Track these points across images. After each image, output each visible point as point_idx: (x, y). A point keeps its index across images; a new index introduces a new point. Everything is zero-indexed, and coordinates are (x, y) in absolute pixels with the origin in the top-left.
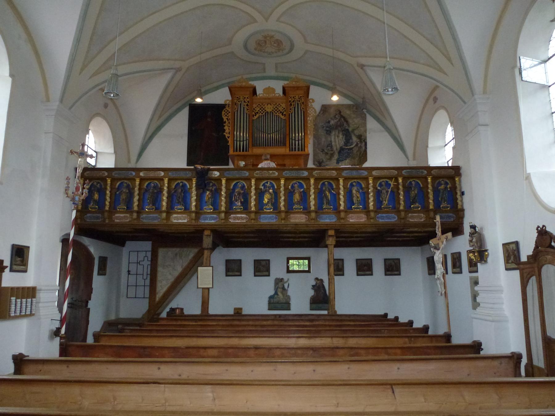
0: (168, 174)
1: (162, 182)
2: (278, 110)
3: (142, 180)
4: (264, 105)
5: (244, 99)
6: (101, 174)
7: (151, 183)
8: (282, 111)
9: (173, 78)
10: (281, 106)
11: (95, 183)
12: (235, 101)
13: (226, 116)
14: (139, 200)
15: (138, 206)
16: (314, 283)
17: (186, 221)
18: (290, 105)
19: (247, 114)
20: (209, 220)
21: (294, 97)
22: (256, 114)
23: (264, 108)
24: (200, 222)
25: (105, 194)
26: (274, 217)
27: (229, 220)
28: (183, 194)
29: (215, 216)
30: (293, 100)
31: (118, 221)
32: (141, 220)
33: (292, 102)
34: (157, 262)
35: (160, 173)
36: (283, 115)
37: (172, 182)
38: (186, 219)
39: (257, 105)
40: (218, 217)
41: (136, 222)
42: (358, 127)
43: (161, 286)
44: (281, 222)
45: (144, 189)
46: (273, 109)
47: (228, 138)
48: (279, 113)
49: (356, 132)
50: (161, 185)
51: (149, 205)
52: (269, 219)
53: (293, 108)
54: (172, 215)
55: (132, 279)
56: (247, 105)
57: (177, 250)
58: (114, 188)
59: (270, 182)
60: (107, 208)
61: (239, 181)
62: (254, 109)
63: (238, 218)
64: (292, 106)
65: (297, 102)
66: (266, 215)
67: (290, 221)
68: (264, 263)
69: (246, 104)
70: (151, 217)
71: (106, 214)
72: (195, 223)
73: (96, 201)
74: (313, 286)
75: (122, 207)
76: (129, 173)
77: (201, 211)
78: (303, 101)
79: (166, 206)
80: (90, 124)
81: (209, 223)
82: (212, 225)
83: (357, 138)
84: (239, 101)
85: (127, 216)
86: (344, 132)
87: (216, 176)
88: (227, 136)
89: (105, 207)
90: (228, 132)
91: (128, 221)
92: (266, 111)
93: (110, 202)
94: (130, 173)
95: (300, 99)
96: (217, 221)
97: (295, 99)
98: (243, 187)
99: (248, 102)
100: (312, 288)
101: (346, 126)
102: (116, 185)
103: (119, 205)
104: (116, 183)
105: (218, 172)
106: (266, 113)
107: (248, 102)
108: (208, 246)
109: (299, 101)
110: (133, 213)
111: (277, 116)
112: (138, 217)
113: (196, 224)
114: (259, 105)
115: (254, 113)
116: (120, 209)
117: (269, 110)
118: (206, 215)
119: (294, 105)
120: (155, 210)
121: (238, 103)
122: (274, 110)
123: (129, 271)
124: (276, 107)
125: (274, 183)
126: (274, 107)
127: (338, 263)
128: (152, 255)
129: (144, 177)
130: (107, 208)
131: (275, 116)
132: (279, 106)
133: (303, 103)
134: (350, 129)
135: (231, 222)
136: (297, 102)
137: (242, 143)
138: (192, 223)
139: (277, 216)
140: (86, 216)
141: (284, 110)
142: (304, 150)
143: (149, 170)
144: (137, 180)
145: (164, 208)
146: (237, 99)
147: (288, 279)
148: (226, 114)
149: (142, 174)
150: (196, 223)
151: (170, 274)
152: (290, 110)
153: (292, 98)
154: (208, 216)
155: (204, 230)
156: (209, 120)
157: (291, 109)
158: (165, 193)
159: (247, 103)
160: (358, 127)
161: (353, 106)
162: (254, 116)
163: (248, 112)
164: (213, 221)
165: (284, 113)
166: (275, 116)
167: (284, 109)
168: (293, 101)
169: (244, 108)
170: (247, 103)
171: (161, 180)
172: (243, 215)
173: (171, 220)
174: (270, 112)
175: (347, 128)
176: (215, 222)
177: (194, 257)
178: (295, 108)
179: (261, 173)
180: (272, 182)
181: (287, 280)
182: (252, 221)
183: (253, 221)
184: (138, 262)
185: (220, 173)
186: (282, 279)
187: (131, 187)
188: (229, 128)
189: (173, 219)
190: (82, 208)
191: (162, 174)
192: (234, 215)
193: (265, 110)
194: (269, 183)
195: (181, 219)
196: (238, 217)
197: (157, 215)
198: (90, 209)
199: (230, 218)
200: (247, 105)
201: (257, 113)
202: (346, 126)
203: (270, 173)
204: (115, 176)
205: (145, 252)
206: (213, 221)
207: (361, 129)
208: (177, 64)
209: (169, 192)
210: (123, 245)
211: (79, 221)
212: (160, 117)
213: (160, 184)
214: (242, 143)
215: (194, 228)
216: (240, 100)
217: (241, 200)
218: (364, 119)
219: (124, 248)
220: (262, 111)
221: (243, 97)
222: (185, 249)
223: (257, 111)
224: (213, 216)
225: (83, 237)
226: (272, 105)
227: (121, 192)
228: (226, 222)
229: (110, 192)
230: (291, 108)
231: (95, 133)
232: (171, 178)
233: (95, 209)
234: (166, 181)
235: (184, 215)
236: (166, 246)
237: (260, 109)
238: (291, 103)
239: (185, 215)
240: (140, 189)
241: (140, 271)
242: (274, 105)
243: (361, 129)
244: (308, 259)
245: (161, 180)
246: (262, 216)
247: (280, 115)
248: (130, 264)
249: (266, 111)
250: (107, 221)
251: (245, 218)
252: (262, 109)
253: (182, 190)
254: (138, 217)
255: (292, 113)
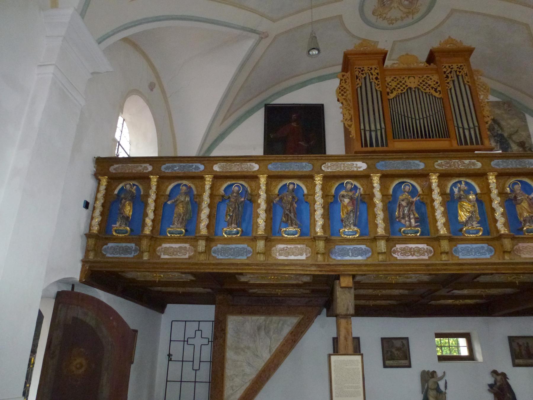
0: (267, 167)
1: (253, 184)
2: (427, 85)
3: (218, 178)
4: (404, 78)
5: (370, 71)
6: (140, 168)
7: (232, 185)
8: (434, 86)
9: (252, 50)
10: (431, 79)
11: (128, 186)
12: (357, 73)
13: (343, 95)
14: (209, 217)
15: (208, 227)
16: (491, 380)
17: (304, 257)
18: (445, 78)
19: (376, 91)
20: (350, 254)
21: (449, 67)
22: (392, 90)
23: (403, 82)
24: (334, 259)
25: (146, 204)
26: (486, 248)
27: (392, 256)
28: (296, 205)
29: (363, 247)
30: (450, 70)
31: (166, 257)
32: (213, 255)
33: (448, 73)
34: (224, 341)
35: (250, 164)
36: (436, 90)
37: (274, 184)
38: (304, 254)
39: (392, 78)
40: (369, 249)
41: (202, 258)
42: (517, 131)
43: (232, 387)
44: (504, 259)
45: (218, 195)
46: (419, 83)
47: (349, 128)
48: (429, 90)
49: (514, 137)
50: (251, 190)
51: (229, 224)
52: (475, 253)
53: (451, 82)
54: (274, 246)
55: (175, 367)
56: (377, 78)
57: (261, 319)
58: (163, 195)
59: (465, 182)
60: (147, 231)
61: (405, 180)
62: (388, 84)
63: (412, 252)
64: (450, 79)
65: (456, 73)
66: (469, 245)
67: (520, 256)
68: (398, 344)
69: (374, 77)
70: (231, 249)
71: (145, 243)
72: (324, 261)
73: (128, 217)
74: (491, 386)
75: (177, 228)
76: (193, 166)
77: (216, 237)
78: (465, 72)
79: (264, 228)
80: (124, 108)
81: (353, 260)
82: (360, 265)
83: (518, 145)
84: (363, 74)
85: (185, 247)
86: (496, 138)
87: (361, 169)
88: (347, 124)
89: (143, 230)
90: (349, 119)
91: (187, 256)
92: (408, 87)
93: (153, 221)
94: (194, 167)
95: (460, 69)
96: (367, 258)
97: (453, 70)
98: (413, 192)
99: (378, 74)
100: (489, 390)
101: (499, 130)
102: (166, 190)
103: (171, 226)
104: (167, 187)
105: (363, 162)
106: (407, 90)
107: (378, 74)
108: (348, 309)
109: (460, 72)
110: (197, 241)
111: (426, 93)
112: (208, 248)
113: (326, 263)
114: (395, 78)
115: (388, 90)
116: (173, 234)
117: (413, 86)
118: (344, 246)
119: (452, 78)
120: (241, 236)
121: (361, 75)
122: (422, 85)
123: (169, 355)
124: (423, 81)
125: (473, 183)
126: (421, 81)
127: (527, 343)
128: (443, 337)
129: (220, 172)
130: (147, 231)
131: (424, 95)
132: (428, 79)
133: (466, 73)
134: (506, 135)
135: (398, 258)
136: (456, 73)
137: (373, 134)
138: (316, 261)
139: (491, 246)
140: (105, 247)
141: (438, 84)
142: (387, 146)
143: (230, 161)
144: (207, 179)
145: (261, 231)
146: (359, 71)
147: (444, 373)
148: (342, 92)
149: (216, 168)
150: (326, 261)
151: (249, 364)
152: (448, 85)
153: (447, 67)
154: (348, 247)
155: (338, 277)
156: (294, 124)
157: (448, 83)
158: (262, 201)
159: (375, 75)
160: (517, 131)
161: (504, 103)
162: (390, 94)
163: (380, 87)
164: (360, 258)
165: (439, 89)
166: (424, 95)
167: (437, 83)
168: (451, 72)
169: (371, 83)
170: (375, 75)
171: (253, 177)
172: (420, 246)
173: (273, 255)
174: (415, 88)
175: (500, 132)
176: (365, 260)
177: (291, 333)
178: (453, 81)
179: (448, 163)
180: (469, 181)
181: (443, 374)
182: (443, 256)
183: (444, 257)
184: (186, 340)
185: (367, 163)
186: (434, 372)
187: (195, 193)
188: (350, 112)
189: (278, 254)
190: (99, 231)
191: (256, 167)
192: (403, 246)
193: (407, 86)
194: (463, 184)
195: (293, 254)
196: (411, 248)
197: (245, 246)
198: (114, 233)
199: (394, 250)
200: (377, 78)
201: (394, 89)
202: (499, 130)
203: (464, 163)
204: (166, 171)
205: (185, 322)
206: (360, 258)
207: (522, 133)
208: (264, 25)
209: (269, 201)
210: (161, 309)
211: (91, 257)
212: (225, 119)
213: (251, 187)
214: (373, 134)
215: (320, 271)
216: (363, 72)
217: (414, 215)
218: (524, 120)
219: (163, 316)
220: (401, 86)
221: (368, 68)
222: (275, 318)
223: (393, 87)
224: (359, 246)
225: (97, 290)
226: (417, 78)
227: (177, 200)
228: (388, 260)
229: (155, 201)
230: (448, 81)
231: (132, 126)
232: (272, 174)
233: (123, 233)
234: (263, 180)
235: (299, 246)
236: (240, 313)
237: (398, 84)
238: (446, 74)
239: (302, 246)
240: (211, 196)
241: (188, 355)
242: (419, 77)
243: (522, 133)
244: (467, 336)
245: (253, 177)
246: (460, 246)
247: (433, 91)
248: (171, 342)
249: (408, 87)
250: (146, 257)
251: (426, 252)
252: (401, 84)
253: (293, 198)
254: (208, 248)
255: (451, 89)
